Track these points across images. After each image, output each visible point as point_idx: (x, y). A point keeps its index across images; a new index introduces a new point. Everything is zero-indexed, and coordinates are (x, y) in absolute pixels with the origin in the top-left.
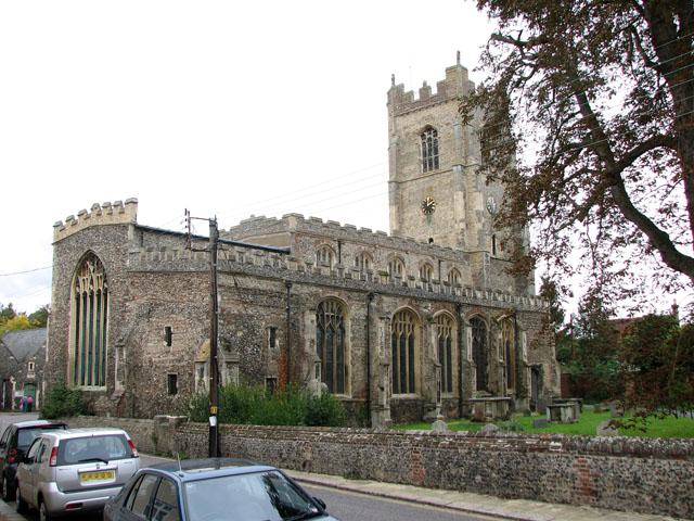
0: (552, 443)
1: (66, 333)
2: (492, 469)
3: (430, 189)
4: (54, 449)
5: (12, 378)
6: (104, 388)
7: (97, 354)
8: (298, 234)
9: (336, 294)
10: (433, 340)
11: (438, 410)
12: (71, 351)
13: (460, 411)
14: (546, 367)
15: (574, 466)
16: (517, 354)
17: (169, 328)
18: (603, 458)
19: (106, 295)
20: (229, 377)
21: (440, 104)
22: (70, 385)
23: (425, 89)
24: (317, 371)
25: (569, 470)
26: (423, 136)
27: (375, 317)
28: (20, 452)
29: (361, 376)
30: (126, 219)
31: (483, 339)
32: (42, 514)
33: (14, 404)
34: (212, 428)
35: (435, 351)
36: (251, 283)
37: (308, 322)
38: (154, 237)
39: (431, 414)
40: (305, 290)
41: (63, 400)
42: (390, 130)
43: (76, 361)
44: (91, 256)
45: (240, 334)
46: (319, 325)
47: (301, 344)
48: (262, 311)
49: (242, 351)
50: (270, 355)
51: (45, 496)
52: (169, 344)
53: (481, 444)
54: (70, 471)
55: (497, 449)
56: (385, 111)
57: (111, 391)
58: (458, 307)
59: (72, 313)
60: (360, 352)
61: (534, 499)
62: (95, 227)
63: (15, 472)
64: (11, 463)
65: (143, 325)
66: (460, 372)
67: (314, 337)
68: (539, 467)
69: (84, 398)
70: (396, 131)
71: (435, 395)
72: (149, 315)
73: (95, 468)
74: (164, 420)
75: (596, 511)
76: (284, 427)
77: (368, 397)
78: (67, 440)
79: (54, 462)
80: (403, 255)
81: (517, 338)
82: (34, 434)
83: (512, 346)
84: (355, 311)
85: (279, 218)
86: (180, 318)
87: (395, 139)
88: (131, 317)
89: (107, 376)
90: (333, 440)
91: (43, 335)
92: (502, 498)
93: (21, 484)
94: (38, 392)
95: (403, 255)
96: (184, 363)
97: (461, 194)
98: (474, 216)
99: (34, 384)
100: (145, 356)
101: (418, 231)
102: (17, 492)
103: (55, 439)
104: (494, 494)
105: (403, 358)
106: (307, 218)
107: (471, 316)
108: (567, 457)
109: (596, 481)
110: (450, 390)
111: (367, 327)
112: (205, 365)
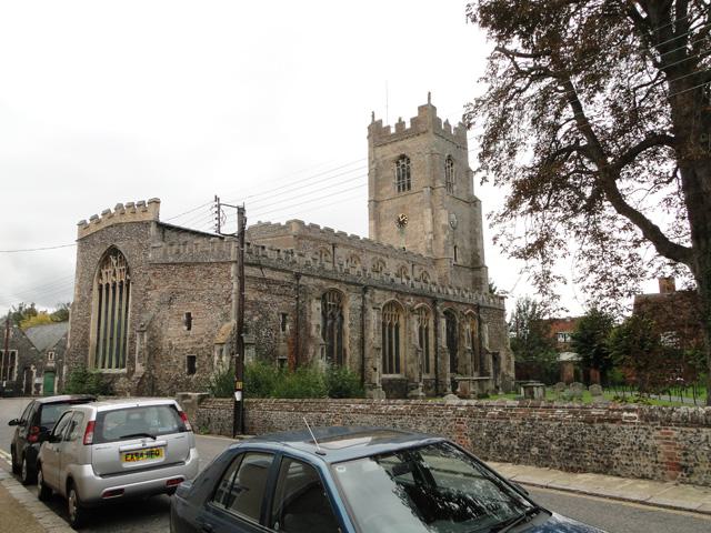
0: (625, 414)
1: (88, 321)
2: (552, 440)
3: (404, 207)
4: (89, 423)
5: (33, 367)
6: (124, 370)
7: (118, 339)
8: (299, 237)
9: (337, 286)
10: (416, 329)
11: (420, 389)
12: (93, 336)
13: (437, 390)
14: (503, 355)
15: (656, 438)
16: (481, 343)
17: (189, 315)
18: (695, 430)
19: (128, 286)
20: (250, 358)
21: (413, 136)
22: (91, 370)
23: (400, 124)
24: (322, 353)
25: (649, 443)
26: (398, 163)
27: (369, 307)
28: (43, 430)
29: (356, 358)
30: (149, 217)
31: (454, 329)
32: (71, 505)
33: (34, 390)
34: (237, 404)
35: (417, 336)
36: (268, 274)
37: (314, 310)
38: (175, 234)
39: (414, 392)
40: (311, 282)
41: (83, 383)
42: (370, 158)
43: (98, 346)
44: (114, 251)
45: (256, 319)
46: (323, 312)
47: (308, 329)
48: (276, 299)
49: (258, 334)
50: (282, 337)
51: (76, 480)
52: (189, 329)
53: (537, 415)
54: (110, 450)
55: (557, 420)
56: (366, 142)
57: (131, 373)
58: (435, 301)
59: (95, 303)
60: (356, 338)
61: (605, 473)
62: (119, 225)
63: (37, 452)
64: (33, 442)
65: (165, 311)
66: (436, 357)
67: (320, 322)
68: (611, 439)
69: (105, 381)
70: (376, 159)
71: (417, 376)
72: (170, 302)
73: (140, 446)
74: (185, 397)
75: (690, 487)
76: (311, 400)
77: (363, 376)
78: (104, 413)
79: (90, 439)
80: (385, 259)
81: (480, 329)
82: (61, 409)
83: (476, 336)
84: (352, 302)
85: (283, 223)
86: (201, 304)
87: (374, 166)
88: (152, 306)
89: (127, 359)
90: (367, 412)
91: (67, 327)
92: (567, 471)
93: (44, 466)
94: (57, 379)
95: (385, 259)
96: (203, 345)
97: (430, 210)
98: (440, 230)
99: (53, 371)
100: (165, 340)
101: (392, 237)
102: (39, 475)
103: (90, 411)
104: (554, 467)
105: (390, 343)
106: (307, 224)
107: (445, 309)
108: (645, 429)
109: (685, 454)
110: (428, 371)
111: (362, 316)
112: (224, 347)
